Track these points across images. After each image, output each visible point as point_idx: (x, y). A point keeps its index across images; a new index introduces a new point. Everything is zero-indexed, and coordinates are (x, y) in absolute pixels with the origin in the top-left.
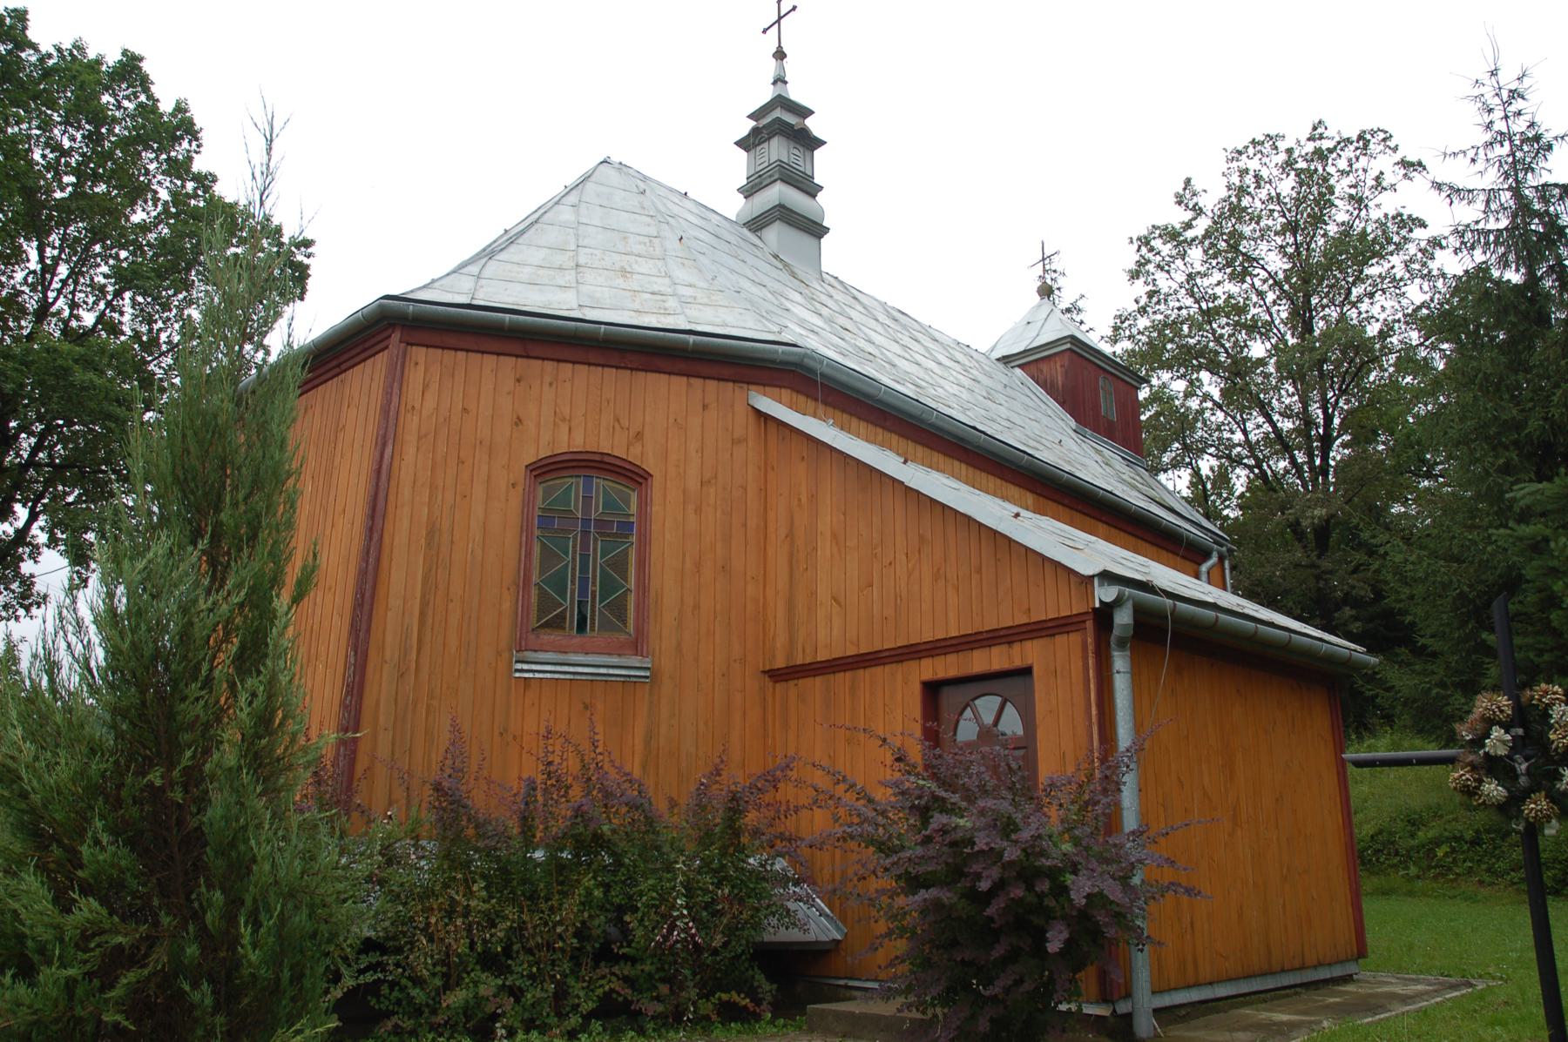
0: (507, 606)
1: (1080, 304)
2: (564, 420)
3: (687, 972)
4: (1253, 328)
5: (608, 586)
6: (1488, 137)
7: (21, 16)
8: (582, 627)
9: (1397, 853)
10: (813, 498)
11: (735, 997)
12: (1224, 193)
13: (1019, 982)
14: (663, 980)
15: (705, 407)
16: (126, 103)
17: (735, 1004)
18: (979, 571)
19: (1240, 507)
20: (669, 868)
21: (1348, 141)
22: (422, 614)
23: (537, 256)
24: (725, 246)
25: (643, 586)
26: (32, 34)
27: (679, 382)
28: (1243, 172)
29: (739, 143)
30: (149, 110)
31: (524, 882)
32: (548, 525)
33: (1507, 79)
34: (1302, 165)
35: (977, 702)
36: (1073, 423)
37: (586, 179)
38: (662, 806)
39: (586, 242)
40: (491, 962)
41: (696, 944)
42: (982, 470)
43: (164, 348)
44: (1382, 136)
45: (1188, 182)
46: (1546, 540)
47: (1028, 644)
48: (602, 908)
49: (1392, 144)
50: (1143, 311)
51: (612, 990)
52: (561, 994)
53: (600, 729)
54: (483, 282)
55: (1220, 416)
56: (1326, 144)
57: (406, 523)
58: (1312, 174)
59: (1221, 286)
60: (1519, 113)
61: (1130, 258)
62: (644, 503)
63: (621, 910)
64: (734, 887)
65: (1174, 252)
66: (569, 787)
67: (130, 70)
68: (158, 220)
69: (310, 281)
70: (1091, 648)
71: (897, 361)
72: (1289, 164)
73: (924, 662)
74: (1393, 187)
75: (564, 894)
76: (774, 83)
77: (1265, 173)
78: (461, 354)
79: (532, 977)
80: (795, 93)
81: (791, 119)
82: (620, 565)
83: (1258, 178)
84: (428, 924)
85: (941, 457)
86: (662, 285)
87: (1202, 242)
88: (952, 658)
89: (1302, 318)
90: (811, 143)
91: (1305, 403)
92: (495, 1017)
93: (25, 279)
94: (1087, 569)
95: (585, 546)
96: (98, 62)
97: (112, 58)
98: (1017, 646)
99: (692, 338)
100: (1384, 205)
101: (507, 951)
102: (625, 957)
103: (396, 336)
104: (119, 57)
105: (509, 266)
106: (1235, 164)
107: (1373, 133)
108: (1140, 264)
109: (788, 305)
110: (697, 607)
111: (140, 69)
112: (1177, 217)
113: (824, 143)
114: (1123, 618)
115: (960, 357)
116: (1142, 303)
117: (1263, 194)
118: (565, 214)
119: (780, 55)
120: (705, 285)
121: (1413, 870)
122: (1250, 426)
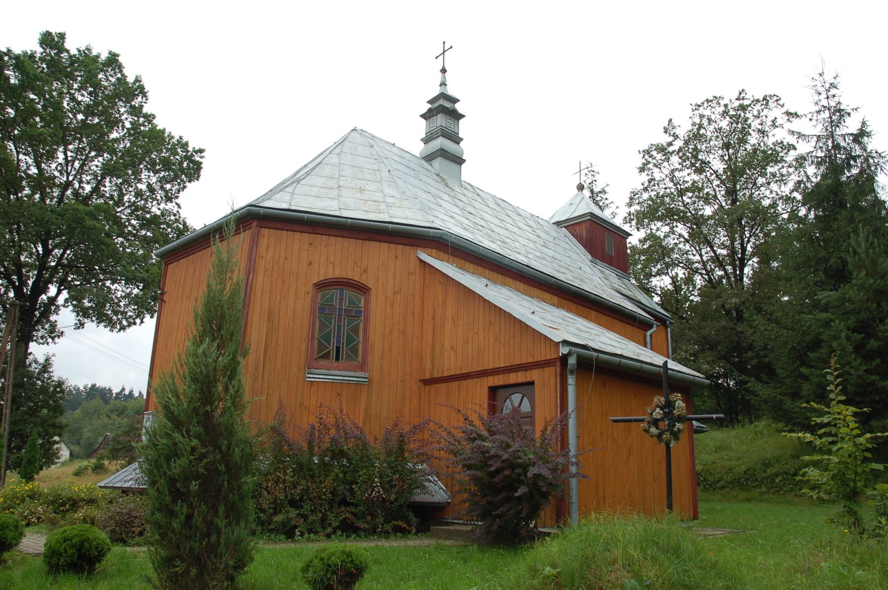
0: (304, 348)
1: (606, 189)
3: (379, 511)
4: (707, 200)
5: (350, 340)
6: (817, 108)
7: (62, 36)
8: (337, 358)
9: (756, 480)
10: (444, 301)
11: (400, 523)
12: (690, 128)
13: (510, 508)
14: (368, 514)
15: (396, 257)
16: (111, 78)
17: (400, 526)
18: (514, 338)
19: (699, 295)
20: (373, 465)
21: (758, 101)
22: (265, 351)
23: (320, 181)
24: (412, 173)
26: (67, 45)
27: (385, 246)
28: (702, 116)
29: (422, 116)
30: (122, 81)
31: (309, 470)
32: (323, 311)
33: (829, 78)
34: (732, 113)
35: (512, 396)
36: (590, 257)
37: (344, 140)
38: (371, 440)
39: (344, 174)
40: (294, 504)
41: (383, 499)
42: (531, 286)
43: (127, 204)
44: (775, 98)
45: (670, 120)
46: (832, 320)
47: (533, 371)
48: (343, 482)
49: (781, 103)
50: (646, 189)
51: (346, 518)
52: (324, 519)
53: (344, 404)
55: (688, 247)
56: (746, 102)
57: (258, 310)
58: (739, 115)
59: (688, 176)
60: (834, 96)
61: (640, 162)
62: (367, 302)
63: (351, 483)
64: (401, 478)
65: (663, 158)
66: (329, 429)
67: (113, 61)
68: (123, 138)
69: (202, 171)
70: (558, 373)
71: (497, 230)
72: (725, 113)
74: (782, 126)
75: (326, 476)
77: (713, 117)
78: (284, 232)
79: (312, 511)
80: (451, 91)
81: (448, 105)
82: (355, 330)
83: (709, 120)
84: (267, 487)
86: (378, 196)
87: (678, 153)
88: (501, 376)
89: (731, 193)
91: (733, 240)
92: (296, 527)
93: (56, 168)
94: (557, 339)
96: (98, 57)
97: (104, 56)
98: (528, 372)
99: (391, 226)
100: (779, 135)
101: (301, 499)
102: (352, 504)
103: (255, 223)
104: (107, 55)
105: (307, 187)
106: (696, 112)
107: (771, 97)
108: (644, 164)
109: (441, 202)
111: (117, 61)
112: (665, 139)
114: (572, 361)
115: (532, 224)
116: (646, 185)
117: (711, 128)
118: (334, 159)
119: (444, 71)
120: (399, 196)
121: (764, 489)
122: (703, 251)
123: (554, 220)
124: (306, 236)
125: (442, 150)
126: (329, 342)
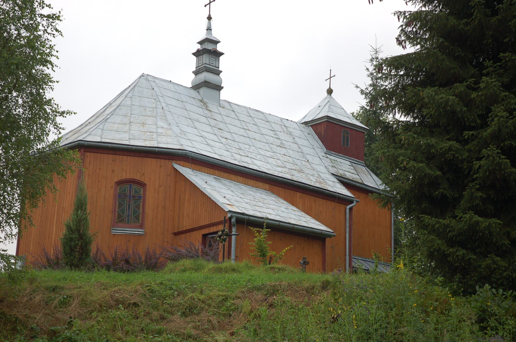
8: (128, 223)
15: (161, 167)
25: (143, 212)
27: (154, 160)
29: (194, 54)
32: (121, 197)
36: (325, 150)
42: (248, 178)
54: (104, 131)
62: (145, 191)
73: (203, 230)
76: (207, 30)
78: (99, 154)
80: (216, 35)
82: (138, 207)
86: (153, 128)
95: (129, 202)
99: (157, 149)
113: (223, 54)
114: (233, 220)
119: (209, 18)
123: (303, 121)
124: (110, 156)
125: (205, 82)
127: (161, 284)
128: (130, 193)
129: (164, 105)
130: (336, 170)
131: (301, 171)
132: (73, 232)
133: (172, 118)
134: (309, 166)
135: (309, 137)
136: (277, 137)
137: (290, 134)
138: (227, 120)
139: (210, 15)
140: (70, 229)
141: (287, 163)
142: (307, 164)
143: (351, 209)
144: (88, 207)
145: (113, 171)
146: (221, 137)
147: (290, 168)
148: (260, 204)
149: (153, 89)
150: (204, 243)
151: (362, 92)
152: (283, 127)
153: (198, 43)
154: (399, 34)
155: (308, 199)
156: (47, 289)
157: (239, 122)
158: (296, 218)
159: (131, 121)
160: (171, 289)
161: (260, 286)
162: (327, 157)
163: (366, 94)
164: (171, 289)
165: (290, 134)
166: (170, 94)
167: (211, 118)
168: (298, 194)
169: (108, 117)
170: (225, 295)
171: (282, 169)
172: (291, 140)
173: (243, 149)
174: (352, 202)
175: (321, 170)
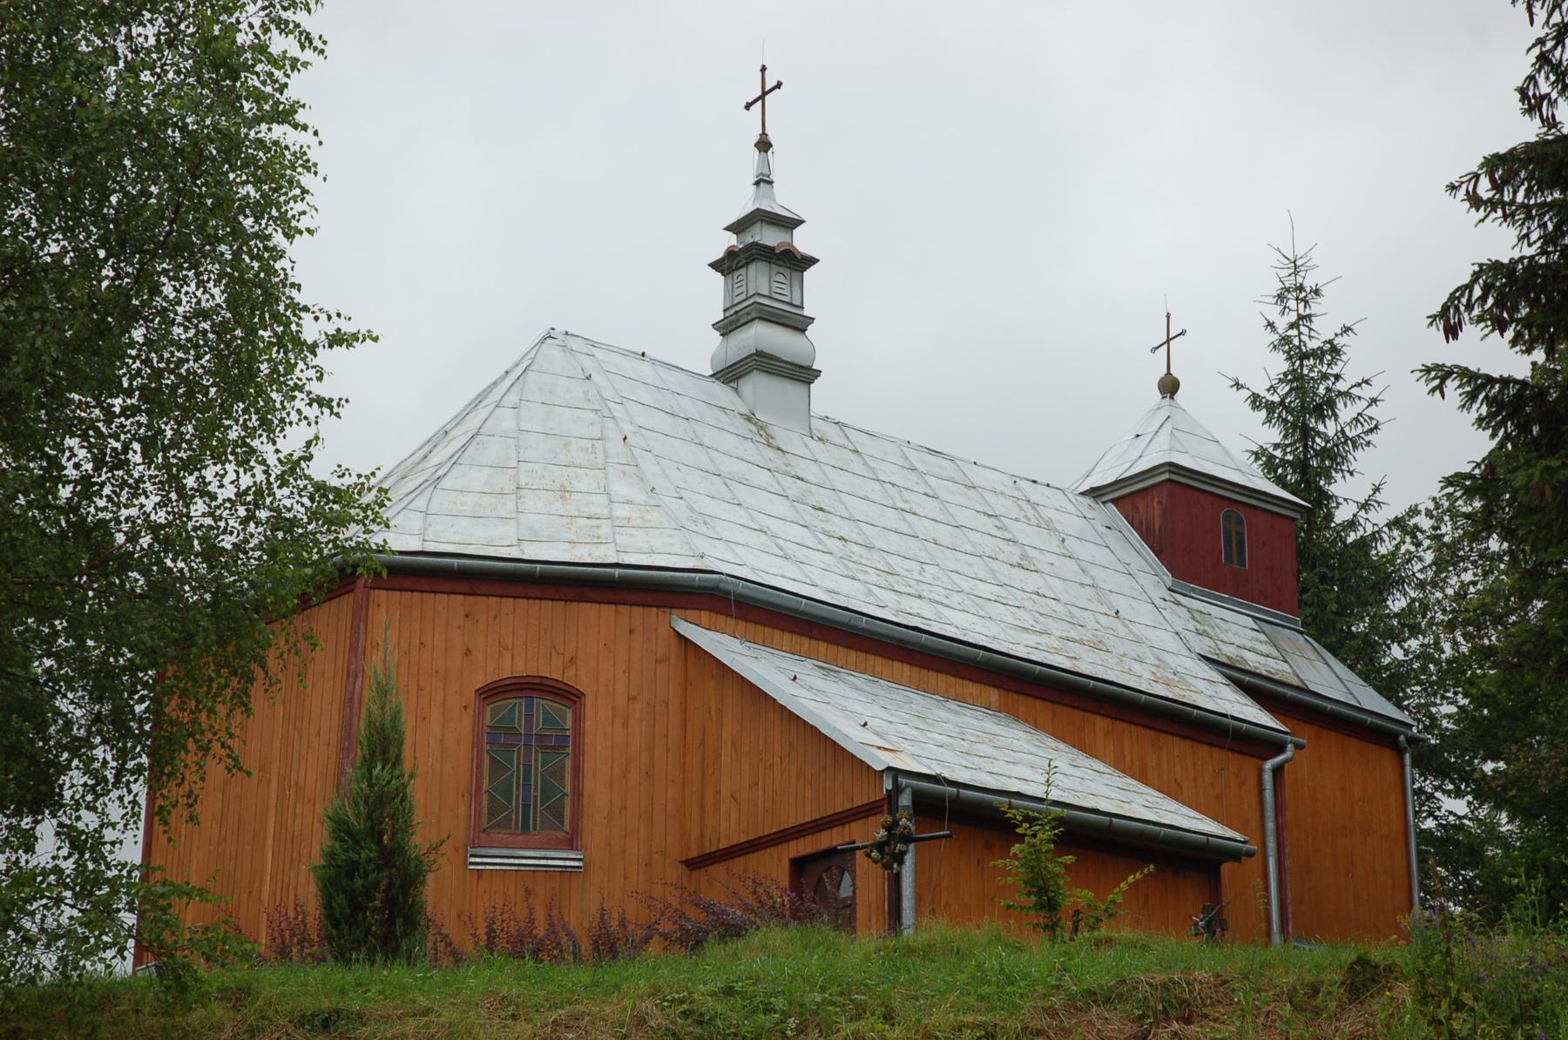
0: (462, 810)
2: (507, 649)
8: (525, 827)
10: (720, 711)
15: (631, 631)
25: (578, 792)
27: (608, 610)
29: (715, 265)
32: (497, 743)
36: (1169, 579)
37: (522, 370)
42: (930, 669)
47: (854, 825)
62: (578, 719)
76: (757, 183)
78: (417, 595)
80: (783, 200)
82: (558, 773)
85: (879, 660)
86: (598, 506)
90: (797, 263)
95: (528, 756)
110: (624, 808)
119: (764, 145)
123: (1085, 487)
125: (760, 354)
126: (508, 798)
127: (729, 991)
128: (529, 726)
129: (628, 429)
130: (1211, 644)
131: (1098, 646)
132: (357, 842)
133: (658, 470)
134: (1122, 632)
135: (1112, 538)
136: (1008, 536)
137: (1049, 526)
138: (840, 480)
139: (764, 133)
140: (348, 833)
141: (1050, 621)
142: (1116, 623)
143: (1278, 771)
144: (407, 754)
145: (468, 652)
146: (825, 533)
147: (1064, 634)
148: (986, 749)
149: (589, 378)
150: (796, 885)
151: (1256, 401)
152: (1023, 504)
153: (727, 229)
154: (1529, 71)
155: (1133, 737)
156: (302, 1021)
157: (877, 485)
158: (1113, 795)
159: (522, 483)
160: (769, 1009)
161: (1110, 990)
162: (1179, 604)
163: (1271, 407)
164: (769, 1009)
165: (1049, 526)
166: (645, 396)
167: (786, 473)
168: (1100, 723)
169: (441, 472)
170: (980, 1026)
171: (1038, 638)
172: (1053, 544)
173: (902, 572)
174: (1280, 748)
175: (1167, 641)
